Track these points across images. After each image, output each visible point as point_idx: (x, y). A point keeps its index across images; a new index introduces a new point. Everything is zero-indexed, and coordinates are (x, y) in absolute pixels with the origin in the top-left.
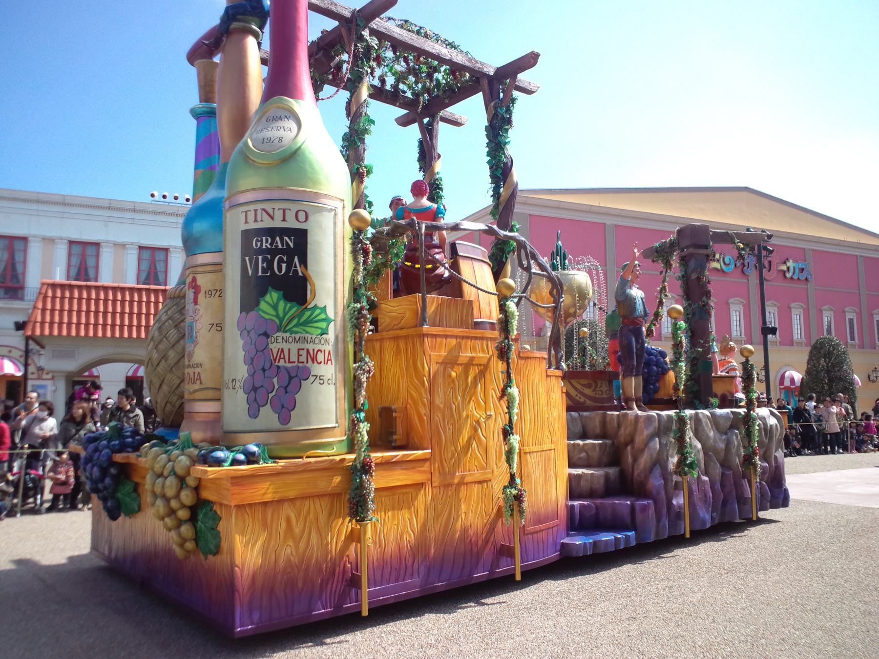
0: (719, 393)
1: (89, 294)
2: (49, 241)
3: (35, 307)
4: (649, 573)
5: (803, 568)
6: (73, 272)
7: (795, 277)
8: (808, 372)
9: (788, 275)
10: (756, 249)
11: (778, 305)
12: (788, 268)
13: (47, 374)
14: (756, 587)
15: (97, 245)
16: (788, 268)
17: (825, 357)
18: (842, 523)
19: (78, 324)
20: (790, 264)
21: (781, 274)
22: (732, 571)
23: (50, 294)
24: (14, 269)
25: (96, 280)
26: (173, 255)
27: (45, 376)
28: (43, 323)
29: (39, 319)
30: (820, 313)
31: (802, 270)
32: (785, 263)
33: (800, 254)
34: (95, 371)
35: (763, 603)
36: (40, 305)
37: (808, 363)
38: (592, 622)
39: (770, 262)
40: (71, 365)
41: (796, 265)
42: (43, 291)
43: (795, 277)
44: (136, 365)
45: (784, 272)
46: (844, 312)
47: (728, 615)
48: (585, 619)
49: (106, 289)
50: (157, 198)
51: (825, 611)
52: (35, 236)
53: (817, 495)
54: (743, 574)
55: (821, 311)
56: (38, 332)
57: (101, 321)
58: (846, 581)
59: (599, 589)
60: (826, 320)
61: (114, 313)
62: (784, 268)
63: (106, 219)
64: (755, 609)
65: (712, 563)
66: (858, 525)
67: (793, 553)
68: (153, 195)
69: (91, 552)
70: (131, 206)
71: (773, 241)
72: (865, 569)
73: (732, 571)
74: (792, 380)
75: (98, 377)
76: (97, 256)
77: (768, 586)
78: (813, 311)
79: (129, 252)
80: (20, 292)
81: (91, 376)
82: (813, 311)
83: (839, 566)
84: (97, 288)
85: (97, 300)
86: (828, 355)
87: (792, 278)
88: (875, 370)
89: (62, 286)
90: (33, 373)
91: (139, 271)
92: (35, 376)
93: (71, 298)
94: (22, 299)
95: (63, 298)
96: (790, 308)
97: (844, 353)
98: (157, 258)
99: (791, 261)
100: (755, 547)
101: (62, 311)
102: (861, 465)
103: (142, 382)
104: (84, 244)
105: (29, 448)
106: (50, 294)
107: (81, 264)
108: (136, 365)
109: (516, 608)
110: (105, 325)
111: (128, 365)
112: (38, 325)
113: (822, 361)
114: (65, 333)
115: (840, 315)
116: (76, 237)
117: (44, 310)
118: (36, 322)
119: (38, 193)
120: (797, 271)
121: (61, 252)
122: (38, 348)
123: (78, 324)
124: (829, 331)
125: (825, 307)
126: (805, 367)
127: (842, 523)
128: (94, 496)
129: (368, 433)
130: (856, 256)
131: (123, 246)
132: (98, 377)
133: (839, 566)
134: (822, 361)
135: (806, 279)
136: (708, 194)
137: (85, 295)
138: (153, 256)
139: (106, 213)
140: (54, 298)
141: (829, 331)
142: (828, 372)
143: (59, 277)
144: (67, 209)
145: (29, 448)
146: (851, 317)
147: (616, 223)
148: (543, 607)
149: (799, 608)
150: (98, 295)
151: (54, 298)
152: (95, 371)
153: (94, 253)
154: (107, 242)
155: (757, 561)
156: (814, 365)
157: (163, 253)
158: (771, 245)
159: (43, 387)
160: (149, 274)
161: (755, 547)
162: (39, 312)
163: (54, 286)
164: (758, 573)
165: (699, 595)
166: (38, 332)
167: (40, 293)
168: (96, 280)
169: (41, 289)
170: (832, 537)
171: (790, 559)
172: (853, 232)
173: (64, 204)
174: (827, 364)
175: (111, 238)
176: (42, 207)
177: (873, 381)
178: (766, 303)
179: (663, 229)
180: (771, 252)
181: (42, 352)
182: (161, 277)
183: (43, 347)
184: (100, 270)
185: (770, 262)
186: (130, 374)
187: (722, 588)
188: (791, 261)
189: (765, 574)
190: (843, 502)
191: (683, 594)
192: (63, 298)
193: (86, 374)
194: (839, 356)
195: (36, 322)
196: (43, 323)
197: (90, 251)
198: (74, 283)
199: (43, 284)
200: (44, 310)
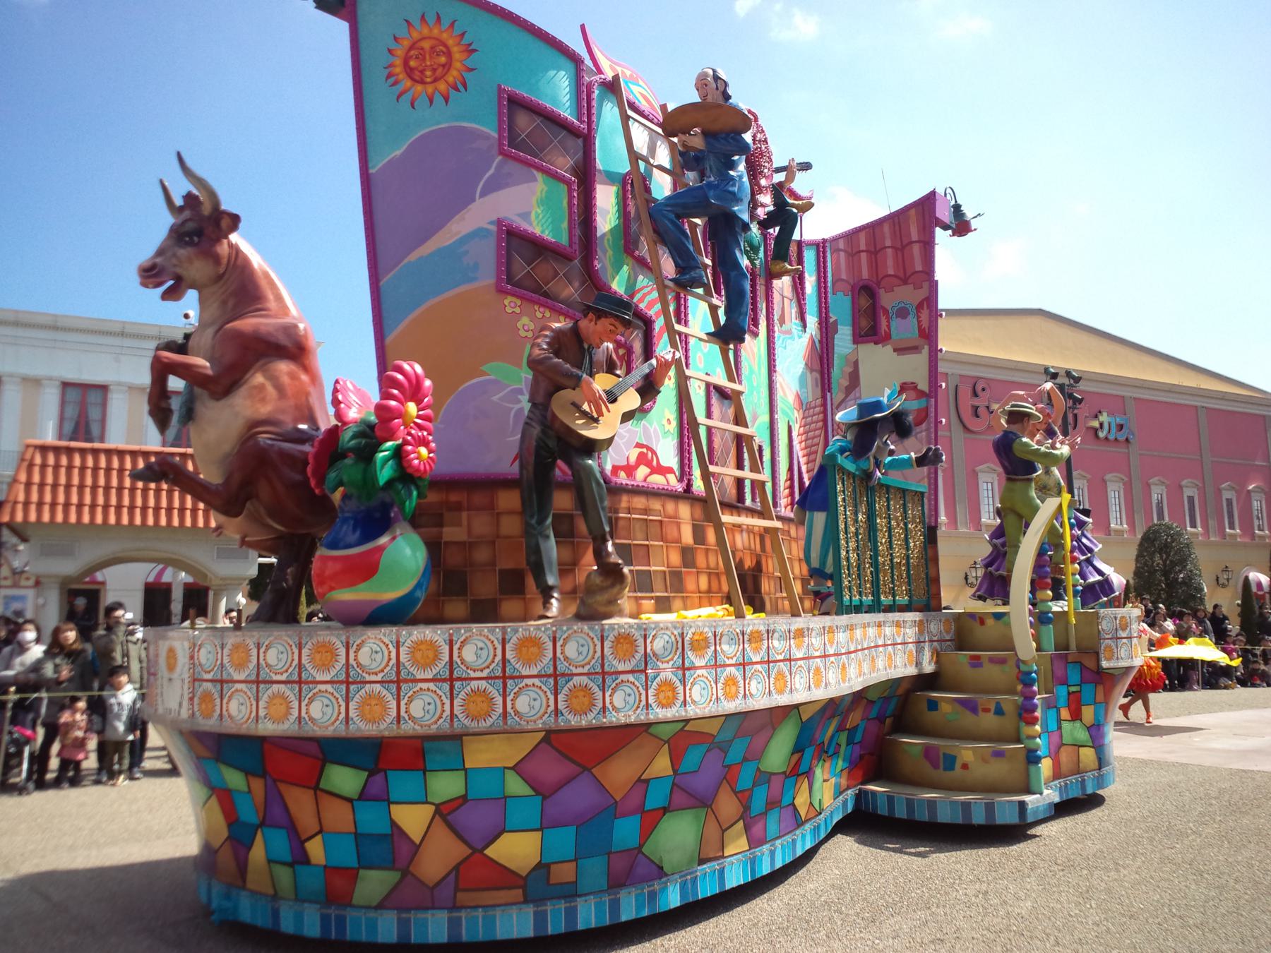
1: (96, 461)
2: (34, 382)
3: (15, 480)
4: (950, 872)
5: (1171, 861)
6: (69, 427)
7: (1111, 437)
8: (1137, 573)
9: (1102, 435)
10: (1072, 398)
11: (1089, 476)
12: (1101, 425)
13: (28, 579)
14: (1109, 891)
15: (103, 389)
16: (1101, 425)
17: (1160, 551)
18: (1213, 794)
19: (93, 506)
20: (1104, 418)
21: (1092, 432)
22: (1069, 866)
23: (38, 460)
25: (102, 440)
27: (23, 583)
28: (27, 504)
29: (21, 497)
30: (1219, 492)
31: (1121, 427)
32: (1096, 416)
33: (1117, 404)
34: (99, 576)
35: (1123, 915)
36: (23, 477)
37: (1137, 561)
38: (881, 947)
39: (1075, 416)
40: (68, 567)
41: (1110, 419)
42: (28, 456)
43: (1111, 437)
44: (161, 566)
45: (1096, 430)
46: (1181, 487)
47: (1077, 935)
48: (869, 943)
49: (121, 453)
51: (1217, 926)
52: (11, 375)
53: (1169, 752)
54: (1085, 872)
55: (1148, 485)
56: (19, 517)
57: (164, 503)
58: (1236, 881)
59: (883, 897)
60: (1155, 497)
61: (81, 487)
62: (1096, 424)
64: (1113, 924)
65: (1037, 855)
66: (1236, 797)
67: (1151, 840)
68: (186, 316)
70: (117, 328)
71: (1082, 386)
72: (1260, 862)
73: (1069, 866)
74: (1259, 585)
75: (103, 583)
76: (104, 405)
77: (1125, 888)
78: (1137, 487)
79: (48, 390)
81: (94, 582)
82: (1137, 487)
83: (1221, 858)
84: (109, 452)
85: (109, 470)
86: (1165, 548)
87: (1106, 438)
88: (1226, 569)
89: (57, 450)
90: (5, 578)
92: (8, 583)
93: (70, 468)
95: (57, 467)
96: (1105, 482)
97: (1188, 546)
99: (1105, 414)
100: (1096, 830)
101: (107, 488)
102: (1231, 707)
104: (85, 387)
105: (17, 692)
106: (38, 460)
107: (79, 416)
108: (161, 566)
109: (767, 929)
110: (119, 507)
111: (147, 567)
112: (20, 507)
113: (1157, 558)
114: (151, 521)
115: (1175, 490)
117: (28, 484)
118: (16, 502)
119: (17, 312)
120: (1114, 430)
121: (50, 399)
122: (14, 540)
123: (67, 505)
124: (1161, 516)
125: (1155, 480)
126: (1132, 566)
127: (1213, 794)
130: (1264, 416)
132: (103, 583)
133: (1221, 858)
134: (1157, 558)
135: (1127, 440)
136: (989, 322)
137: (103, 464)
140: (44, 466)
141: (1161, 516)
142: (1166, 573)
143: (49, 436)
144: (60, 336)
145: (17, 692)
146: (1229, 497)
147: (963, 373)
148: (805, 926)
149: (1177, 922)
150: (109, 462)
151: (44, 466)
152: (99, 576)
153: (99, 400)
154: (119, 384)
155: (1102, 852)
156: (1145, 564)
158: (1079, 392)
159: (21, 598)
160: (77, 425)
161: (1096, 830)
162: (22, 488)
163: (44, 449)
164: (1106, 869)
165: (1029, 904)
166: (19, 517)
167: (23, 460)
168: (102, 440)
169: (24, 454)
170: (1202, 814)
171: (1149, 847)
172: (1184, 371)
173: (55, 328)
174: (1164, 562)
176: (20, 332)
177: (1224, 586)
178: (1075, 473)
179: (999, 377)
180: (1080, 401)
181: (21, 547)
182: (95, 430)
183: (24, 540)
185: (1075, 416)
186: (151, 579)
187: (1060, 893)
188: (1105, 414)
189: (1117, 871)
190: (1208, 761)
191: (1005, 902)
192: (57, 467)
193: (87, 579)
194: (1180, 550)
195: (16, 502)
196: (27, 504)
198: (74, 444)
199: (28, 446)
200: (28, 484)
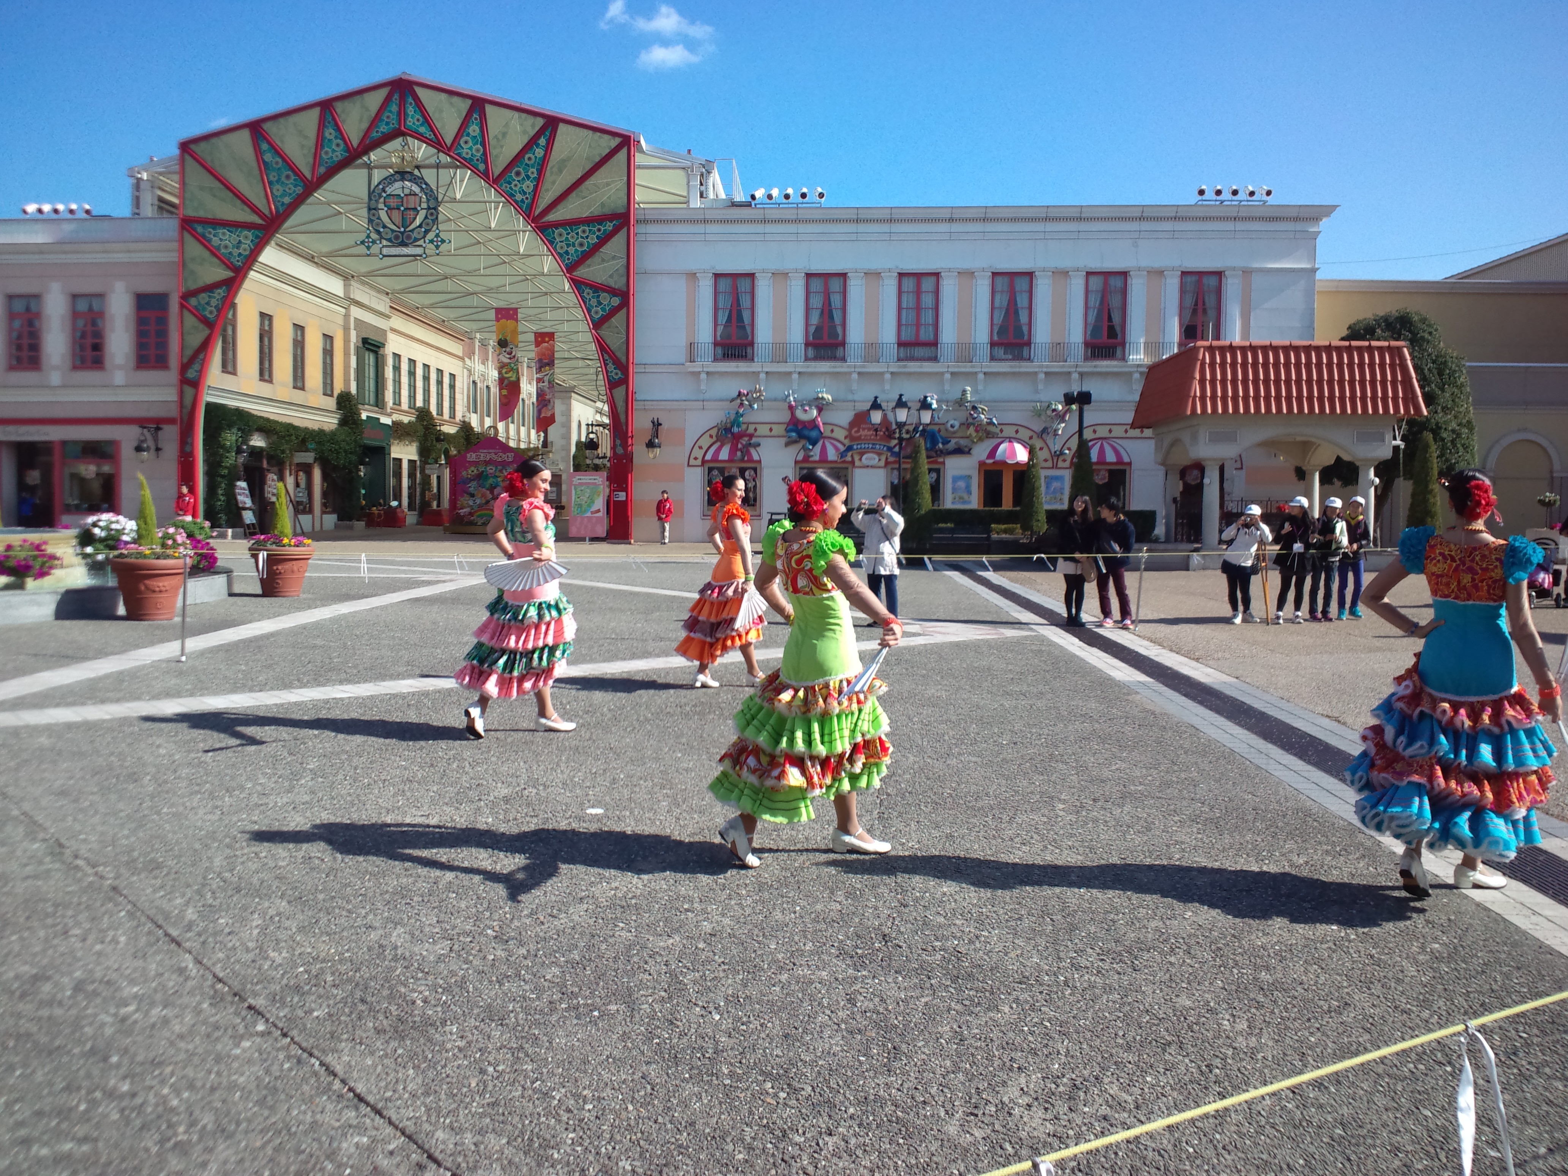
0: (858, 668)
2: (874, 275)
24: (740, 318)
26: (1230, 281)
50: (1210, 195)
63: (1136, 235)
69: (1355, 758)
80: (1025, 350)
91: (1087, 307)
94: (843, 359)
98: (1018, 288)
103: (324, 505)
116: (1096, 265)
128: (833, 684)
129: (1500, 616)
131: (692, 276)
138: (1106, 284)
139: (1134, 226)
157: (748, 281)
175: (1145, 263)
184: (1128, 312)
197: (1021, 284)
